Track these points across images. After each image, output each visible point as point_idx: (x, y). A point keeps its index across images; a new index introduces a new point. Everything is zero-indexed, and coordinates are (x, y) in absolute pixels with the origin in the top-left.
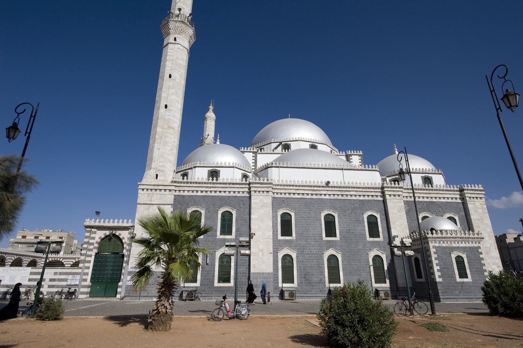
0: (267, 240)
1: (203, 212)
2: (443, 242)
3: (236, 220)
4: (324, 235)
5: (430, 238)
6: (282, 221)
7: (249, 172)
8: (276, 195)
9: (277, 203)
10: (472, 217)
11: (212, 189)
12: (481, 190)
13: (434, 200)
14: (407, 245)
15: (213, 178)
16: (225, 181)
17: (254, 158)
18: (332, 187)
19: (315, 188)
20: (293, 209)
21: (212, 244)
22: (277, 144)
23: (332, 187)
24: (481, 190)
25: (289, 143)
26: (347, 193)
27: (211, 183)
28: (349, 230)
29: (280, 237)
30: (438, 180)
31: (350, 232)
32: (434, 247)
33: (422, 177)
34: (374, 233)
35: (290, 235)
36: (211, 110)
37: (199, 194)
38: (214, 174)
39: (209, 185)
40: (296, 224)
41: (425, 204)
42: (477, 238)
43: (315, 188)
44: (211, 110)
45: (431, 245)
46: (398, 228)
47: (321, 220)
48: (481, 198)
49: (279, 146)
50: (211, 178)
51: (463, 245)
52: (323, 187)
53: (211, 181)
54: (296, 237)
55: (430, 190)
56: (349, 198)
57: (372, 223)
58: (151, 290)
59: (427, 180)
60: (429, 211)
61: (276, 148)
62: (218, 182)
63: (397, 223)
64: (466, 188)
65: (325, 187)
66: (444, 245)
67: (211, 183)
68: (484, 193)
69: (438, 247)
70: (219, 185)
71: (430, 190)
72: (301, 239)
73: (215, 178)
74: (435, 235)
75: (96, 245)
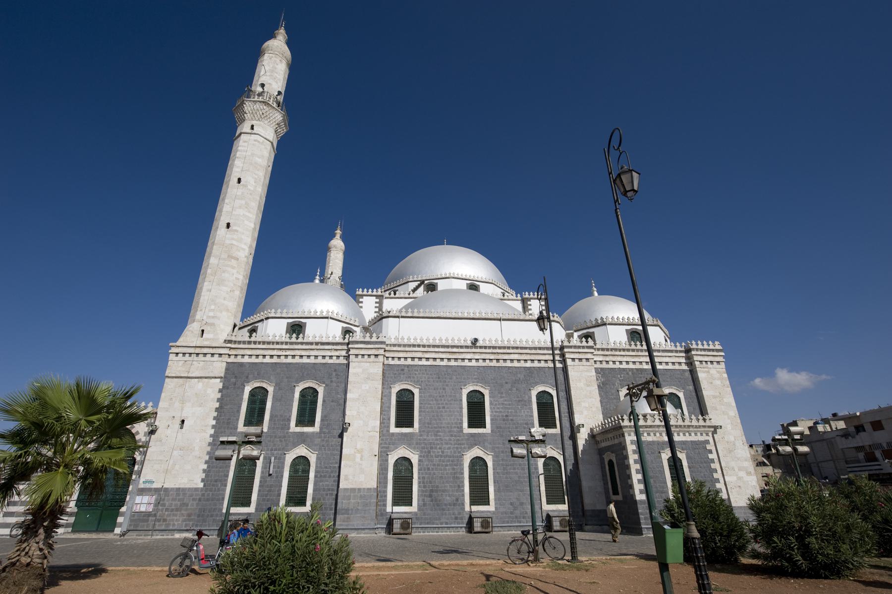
0: (371, 434)
1: (271, 389)
3: (324, 401)
5: (626, 427)
8: (391, 362)
9: (390, 374)
11: (288, 353)
12: (718, 350)
18: (481, 347)
19: (455, 350)
20: (417, 383)
21: (281, 441)
22: (417, 284)
23: (481, 347)
24: (718, 350)
26: (506, 357)
28: (507, 416)
29: (393, 429)
36: (338, 236)
37: (267, 360)
40: (420, 408)
41: (630, 373)
42: (704, 427)
43: (455, 350)
44: (338, 236)
46: (585, 413)
47: (461, 400)
48: (718, 362)
55: (638, 350)
56: (508, 364)
58: (173, 520)
63: (583, 404)
64: (694, 346)
71: (638, 350)
72: (428, 432)
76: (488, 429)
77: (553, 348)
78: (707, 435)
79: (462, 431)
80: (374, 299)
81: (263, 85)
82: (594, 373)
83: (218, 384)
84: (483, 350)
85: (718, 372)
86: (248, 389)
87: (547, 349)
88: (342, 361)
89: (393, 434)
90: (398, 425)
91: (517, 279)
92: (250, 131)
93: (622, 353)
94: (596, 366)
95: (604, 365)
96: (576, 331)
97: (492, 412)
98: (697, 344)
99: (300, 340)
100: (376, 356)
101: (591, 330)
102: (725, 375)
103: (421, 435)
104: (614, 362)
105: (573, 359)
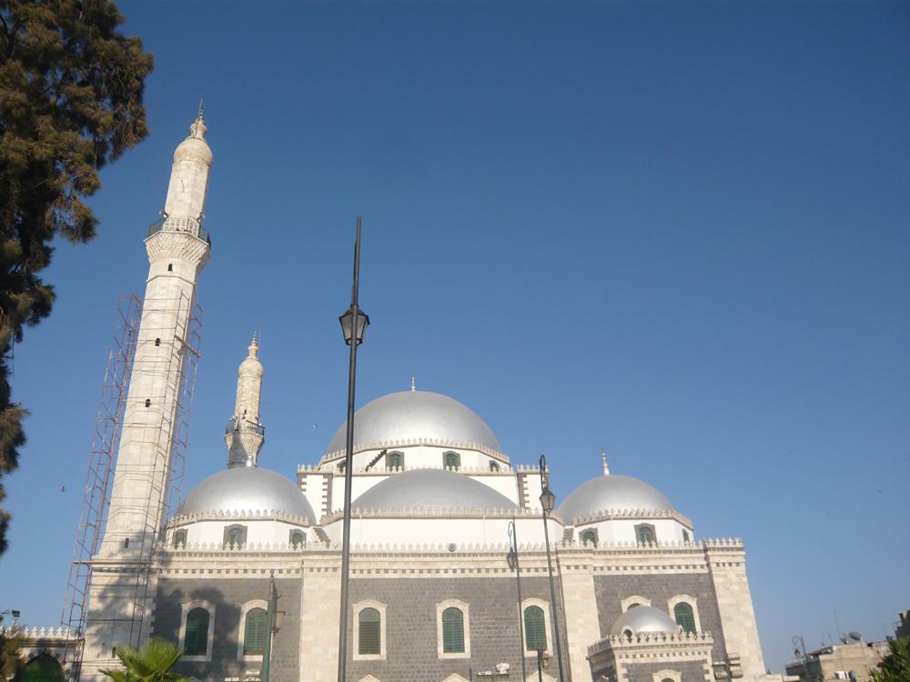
2: (642, 656)
4: (441, 649)
5: (617, 648)
6: (362, 624)
7: (305, 527)
9: (349, 590)
10: (720, 601)
12: (738, 549)
13: (654, 572)
14: (501, 673)
15: (232, 543)
16: (256, 549)
17: (326, 487)
18: (459, 555)
20: (383, 600)
22: (379, 452)
23: (459, 555)
24: (738, 549)
25: (401, 450)
27: (227, 555)
28: (489, 637)
29: (357, 656)
30: (668, 532)
31: (491, 642)
32: (624, 665)
33: (636, 526)
35: (376, 650)
36: (252, 355)
38: (235, 534)
39: (225, 559)
40: (388, 630)
41: (636, 580)
42: (702, 644)
44: (252, 355)
45: (619, 662)
46: (580, 631)
47: (435, 620)
48: (738, 564)
49: (380, 457)
50: (228, 545)
51: (677, 659)
52: (442, 555)
53: (228, 550)
54: (388, 654)
55: (646, 552)
57: (370, 644)
59: (646, 533)
60: (642, 594)
61: (372, 464)
62: (242, 551)
63: (579, 621)
64: (711, 545)
65: (448, 555)
66: (643, 661)
67: (227, 555)
68: (743, 553)
69: (631, 665)
70: (243, 558)
71: (646, 552)
72: (397, 658)
73: (236, 545)
74: (634, 643)
76: (466, 654)
77: (548, 553)
78: (706, 653)
79: (437, 657)
80: (321, 479)
82: (592, 583)
83: (118, 463)
84: (462, 558)
85: (738, 575)
86: (441, 609)
87: (543, 554)
88: (705, 571)
89: (356, 662)
90: (362, 651)
91: (510, 443)
93: (627, 556)
94: (596, 573)
95: (606, 573)
96: (576, 526)
97: (472, 633)
98: (715, 542)
101: (593, 526)
102: (745, 579)
103: (389, 663)
105: (568, 567)
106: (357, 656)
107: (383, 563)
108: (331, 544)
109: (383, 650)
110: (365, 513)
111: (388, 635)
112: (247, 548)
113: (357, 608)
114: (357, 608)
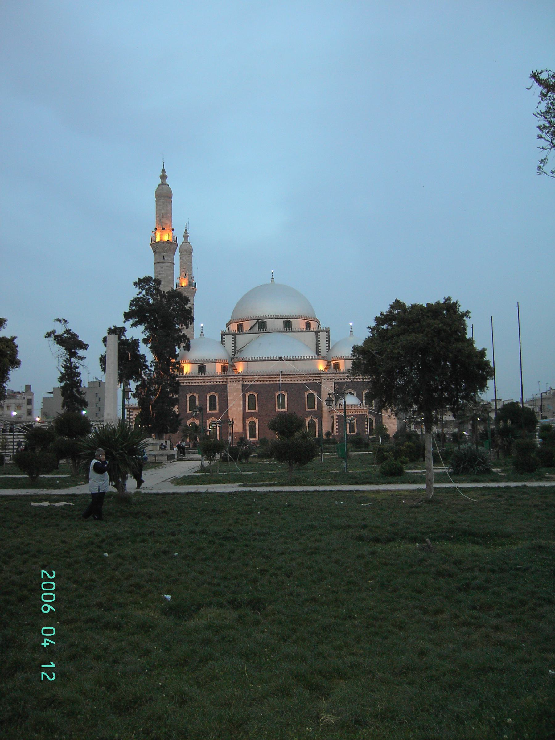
1: (197, 396)
8: (245, 383)
20: (256, 392)
32: (336, 415)
34: (311, 405)
38: (202, 369)
56: (296, 382)
57: (252, 406)
75: (134, 419)
81: (138, 295)
86: (188, 397)
88: (224, 383)
92: (163, 261)
99: (288, 331)
100: (239, 381)
104: (282, 381)
106: (247, 411)
107: (257, 378)
108: (143, 485)
109: (257, 409)
110: (262, 331)
111: (278, 492)
112: (207, 374)
113: (247, 394)
114: (247, 394)
